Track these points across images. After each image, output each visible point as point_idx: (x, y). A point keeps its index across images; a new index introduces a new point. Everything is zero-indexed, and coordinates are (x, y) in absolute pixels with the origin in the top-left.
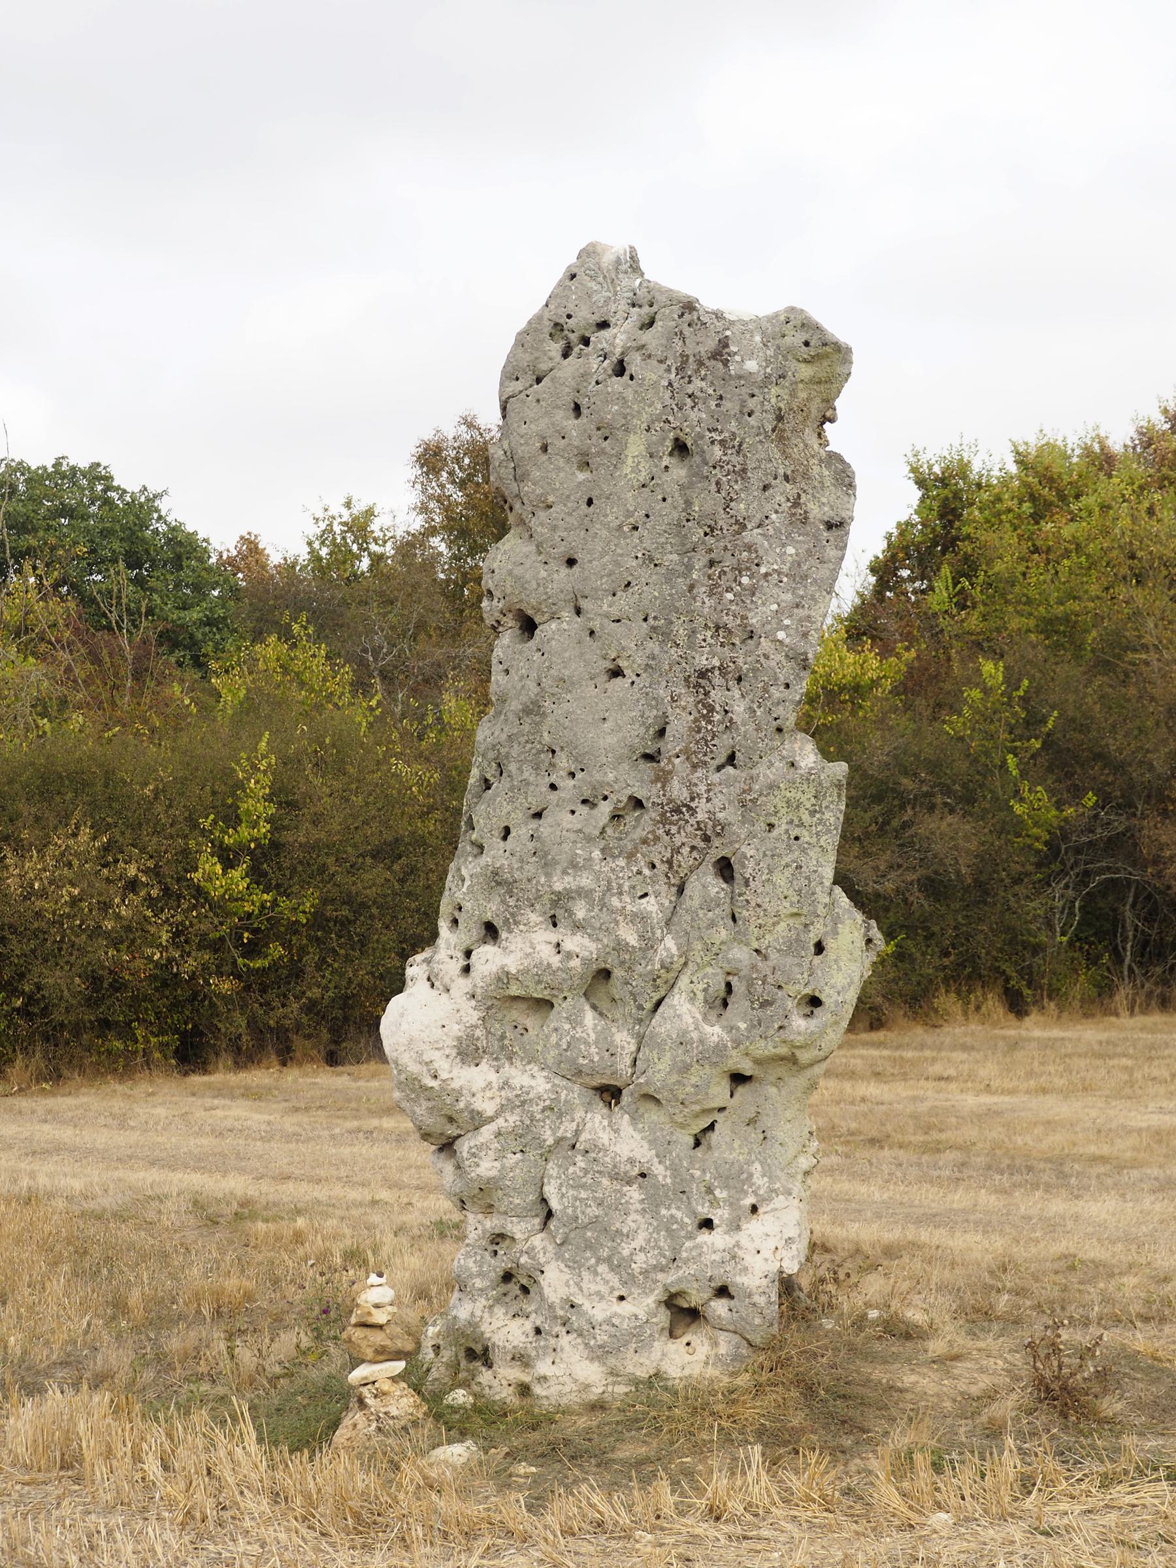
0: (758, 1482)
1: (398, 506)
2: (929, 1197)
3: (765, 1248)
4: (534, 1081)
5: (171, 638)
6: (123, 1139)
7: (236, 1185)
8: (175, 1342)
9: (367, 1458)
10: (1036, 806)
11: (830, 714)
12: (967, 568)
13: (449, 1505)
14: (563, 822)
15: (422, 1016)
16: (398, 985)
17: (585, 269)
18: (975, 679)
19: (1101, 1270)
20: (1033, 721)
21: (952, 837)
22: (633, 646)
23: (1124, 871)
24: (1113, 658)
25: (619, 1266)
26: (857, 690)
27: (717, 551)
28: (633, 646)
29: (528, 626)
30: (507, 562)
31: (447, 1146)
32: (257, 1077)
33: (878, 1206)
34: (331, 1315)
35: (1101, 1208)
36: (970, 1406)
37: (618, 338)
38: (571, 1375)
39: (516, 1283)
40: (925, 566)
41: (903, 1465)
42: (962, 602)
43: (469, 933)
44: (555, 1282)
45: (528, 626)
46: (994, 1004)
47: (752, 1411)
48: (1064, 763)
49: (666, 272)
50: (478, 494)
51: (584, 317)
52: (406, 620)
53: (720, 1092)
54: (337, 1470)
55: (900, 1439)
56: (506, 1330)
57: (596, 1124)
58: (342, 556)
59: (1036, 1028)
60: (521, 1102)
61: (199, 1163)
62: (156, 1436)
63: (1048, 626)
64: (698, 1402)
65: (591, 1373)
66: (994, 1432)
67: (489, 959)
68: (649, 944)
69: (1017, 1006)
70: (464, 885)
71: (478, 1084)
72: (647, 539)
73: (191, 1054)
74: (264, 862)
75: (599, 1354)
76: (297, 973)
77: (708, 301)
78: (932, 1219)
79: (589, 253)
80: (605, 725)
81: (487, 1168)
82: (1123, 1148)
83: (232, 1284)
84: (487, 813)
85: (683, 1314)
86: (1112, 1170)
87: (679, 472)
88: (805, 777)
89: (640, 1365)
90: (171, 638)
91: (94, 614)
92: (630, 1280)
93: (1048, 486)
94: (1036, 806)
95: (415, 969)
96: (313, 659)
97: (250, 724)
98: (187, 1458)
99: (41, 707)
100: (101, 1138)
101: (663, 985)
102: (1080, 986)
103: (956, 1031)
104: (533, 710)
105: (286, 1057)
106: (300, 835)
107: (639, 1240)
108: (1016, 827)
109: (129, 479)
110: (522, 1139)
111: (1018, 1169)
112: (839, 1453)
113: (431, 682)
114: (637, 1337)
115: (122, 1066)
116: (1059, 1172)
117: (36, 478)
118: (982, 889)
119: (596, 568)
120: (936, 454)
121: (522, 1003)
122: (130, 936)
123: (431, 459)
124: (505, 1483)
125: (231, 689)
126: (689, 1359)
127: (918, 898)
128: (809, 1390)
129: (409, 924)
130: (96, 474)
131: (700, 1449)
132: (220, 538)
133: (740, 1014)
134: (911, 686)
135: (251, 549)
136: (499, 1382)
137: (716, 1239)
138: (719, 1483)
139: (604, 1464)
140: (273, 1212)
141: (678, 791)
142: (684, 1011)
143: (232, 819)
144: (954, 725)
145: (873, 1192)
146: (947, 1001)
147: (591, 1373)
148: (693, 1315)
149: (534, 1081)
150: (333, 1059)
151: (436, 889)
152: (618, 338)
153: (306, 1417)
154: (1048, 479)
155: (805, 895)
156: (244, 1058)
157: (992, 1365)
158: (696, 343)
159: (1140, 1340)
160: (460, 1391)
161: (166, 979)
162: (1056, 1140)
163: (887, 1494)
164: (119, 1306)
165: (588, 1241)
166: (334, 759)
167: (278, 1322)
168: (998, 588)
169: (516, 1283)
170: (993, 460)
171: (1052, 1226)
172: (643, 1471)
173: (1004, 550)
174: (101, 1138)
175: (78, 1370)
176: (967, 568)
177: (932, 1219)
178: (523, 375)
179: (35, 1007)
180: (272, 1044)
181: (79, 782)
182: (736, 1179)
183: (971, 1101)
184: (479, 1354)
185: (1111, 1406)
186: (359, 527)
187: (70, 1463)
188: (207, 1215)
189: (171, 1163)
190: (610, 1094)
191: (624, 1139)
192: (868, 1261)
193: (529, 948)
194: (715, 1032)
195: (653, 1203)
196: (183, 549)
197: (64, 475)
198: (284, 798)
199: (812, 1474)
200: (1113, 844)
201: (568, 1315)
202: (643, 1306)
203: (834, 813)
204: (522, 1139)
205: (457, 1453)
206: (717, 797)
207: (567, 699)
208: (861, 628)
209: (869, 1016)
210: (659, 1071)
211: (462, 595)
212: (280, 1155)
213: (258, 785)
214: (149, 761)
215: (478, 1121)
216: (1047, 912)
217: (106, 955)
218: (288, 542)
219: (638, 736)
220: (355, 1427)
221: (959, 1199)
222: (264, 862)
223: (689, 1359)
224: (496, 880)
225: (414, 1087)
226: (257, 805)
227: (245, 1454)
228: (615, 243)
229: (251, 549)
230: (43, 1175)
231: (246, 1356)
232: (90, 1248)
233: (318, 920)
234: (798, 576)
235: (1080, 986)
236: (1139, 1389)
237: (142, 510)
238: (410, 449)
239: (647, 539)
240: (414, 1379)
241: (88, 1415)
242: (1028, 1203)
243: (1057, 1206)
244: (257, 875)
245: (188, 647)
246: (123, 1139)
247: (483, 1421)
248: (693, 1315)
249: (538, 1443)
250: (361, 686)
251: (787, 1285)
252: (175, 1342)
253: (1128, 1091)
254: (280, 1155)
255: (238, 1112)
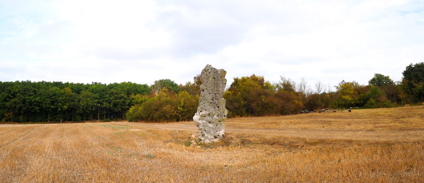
0: (221, 148)
1: (192, 81)
2: (234, 130)
3: (221, 133)
4: (204, 122)
5: (175, 91)
6: (173, 126)
7: (182, 129)
8: (178, 140)
9: (193, 147)
10: (243, 102)
11: (226, 96)
12: (238, 86)
13: (199, 150)
14: (206, 104)
15: (196, 117)
16: (194, 115)
17: (207, 66)
18: (238, 93)
19: (245, 134)
20: (243, 96)
21: (236, 104)
22: (210, 91)
23: (249, 107)
24: (248, 92)
25: (211, 134)
26: (229, 94)
27: (216, 85)
28: (210, 91)
29: (203, 91)
30: (202, 86)
31: (198, 126)
32: (183, 122)
33: (229, 130)
34: (189, 138)
35: (246, 130)
36: (237, 143)
37: (209, 71)
38: (207, 141)
39: (203, 135)
40: (235, 85)
41: (232, 147)
42: (237, 88)
43: (199, 112)
44: (206, 135)
45: (203, 91)
46: (239, 116)
47: (220, 144)
48: (245, 99)
49: (213, 66)
50: (199, 80)
51: (207, 69)
52: (194, 89)
53: (218, 122)
54: (191, 147)
55: (232, 145)
56: (203, 138)
57: (209, 124)
58: (188, 85)
59: (243, 118)
60: (203, 123)
61: (179, 128)
62: (177, 146)
63: (244, 90)
64: (217, 143)
65: (209, 141)
66: (238, 145)
67: (201, 113)
68: (213, 112)
69: (241, 116)
70: (199, 108)
71: (200, 122)
72: (211, 84)
73: (178, 121)
74: (183, 107)
75: (209, 140)
76: (185, 115)
77: (216, 68)
78: (234, 131)
79: (207, 65)
80: (209, 97)
81: (201, 127)
82: (248, 126)
83: (182, 136)
84: (200, 104)
85: (215, 137)
86: (247, 128)
87: (214, 80)
88: (223, 102)
89: (212, 141)
90: (175, 91)
91: (170, 90)
92: (211, 135)
93: (244, 80)
94: (243, 102)
95: (195, 114)
96: (186, 93)
97: (182, 97)
98: (180, 147)
99: (166, 96)
100: (171, 126)
101: (214, 115)
102: (246, 115)
103: (237, 118)
104: (204, 96)
105: (185, 121)
106: (185, 105)
107: (212, 132)
108: (241, 104)
109: (172, 80)
110: (204, 125)
111: (240, 128)
112: (227, 146)
113: (195, 94)
114: (212, 139)
115: (173, 121)
116: (243, 128)
117: (165, 80)
118: (239, 108)
119: (208, 86)
120: (235, 77)
121: (203, 116)
122: (173, 112)
123: (195, 78)
124: (203, 148)
125: (180, 95)
126: (216, 140)
127: (234, 109)
128: (225, 142)
129: (194, 111)
130: (169, 80)
131: (217, 146)
132: (179, 84)
133: (219, 117)
134: (233, 94)
135: (181, 85)
136: (202, 142)
137: (218, 132)
138: (218, 148)
139: (210, 147)
140: (184, 131)
141: (214, 102)
142: (215, 117)
143: (181, 104)
144: (236, 97)
145: (230, 129)
146: (236, 116)
147: (209, 141)
148: (216, 137)
149: (204, 122)
150: (188, 121)
151: (197, 108)
152: (209, 71)
153: (188, 144)
154: (244, 79)
155: (223, 108)
156: (182, 121)
157: (238, 140)
158: (215, 71)
159: (247, 138)
160: (199, 142)
161: (176, 115)
162: (243, 126)
163: (231, 149)
164: (174, 137)
165: (208, 132)
166: (188, 100)
167: (185, 138)
168: (240, 87)
169: (203, 135)
170: (240, 78)
171: (242, 131)
172: (213, 148)
173: (240, 84)
174: (171, 126)
175: (171, 141)
176: (238, 86)
177: (234, 131)
178: (203, 73)
179: (166, 117)
180: (184, 120)
181: (169, 102)
182: (219, 128)
183: (237, 123)
184: (201, 140)
185: (245, 143)
186: (189, 83)
187: (171, 147)
188: (180, 131)
189: (177, 128)
190: (210, 122)
191: (211, 125)
192: (229, 134)
193: (204, 112)
194: (218, 118)
195: (213, 130)
196: (176, 85)
197: (167, 80)
198: (184, 102)
199: (225, 148)
200: (248, 105)
201: (207, 137)
202: (213, 137)
203: (225, 103)
204: (204, 125)
205: (199, 147)
206: (217, 102)
207: (206, 96)
208: (230, 90)
209: (229, 117)
210: (214, 121)
211: (198, 88)
212: (185, 127)
213: (182, 102)
214: (174, 100)
215: (200, 124)
216: (244, 110)
217: (171, 114)
218: (184, 84)
219: (211, 98)
220: (192, 145)
221: (236, 130)
222: (183, 107)
223: (216, 140)
224: (201, 108)
225: (195, 122)
226: (182, 103)
227: (184, 147)
228: (210, 64)
229: (181, 85)
230: (167, 129)
231: (183, 141)
232: (171, 134)
233: (187, 111)
234: (222, 87)
235: (246, 115)
236: (247, 142)
237: (173, 82)
238: (193, 77)
239: (211, 84)
240: (196, 142)
241: (172, 144)
242: (241, 130)
243: (243, 130)
244: (182, 108)
245: (177, 92)
246: (173, 126)
247: (201, 145)
248: (216, 137)
249: (205, 146)
250: (190, 94)
251: (223, 135)
252: (178, 140)
253: (249, 122)
254: (185, 127)
255: (181, 125)
